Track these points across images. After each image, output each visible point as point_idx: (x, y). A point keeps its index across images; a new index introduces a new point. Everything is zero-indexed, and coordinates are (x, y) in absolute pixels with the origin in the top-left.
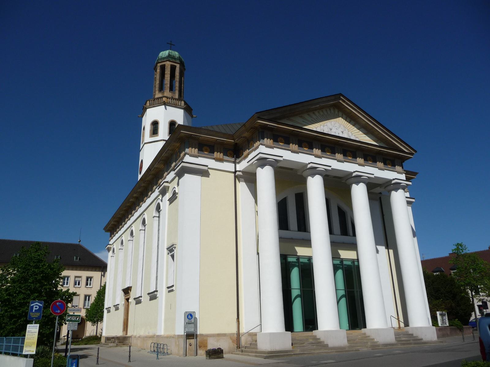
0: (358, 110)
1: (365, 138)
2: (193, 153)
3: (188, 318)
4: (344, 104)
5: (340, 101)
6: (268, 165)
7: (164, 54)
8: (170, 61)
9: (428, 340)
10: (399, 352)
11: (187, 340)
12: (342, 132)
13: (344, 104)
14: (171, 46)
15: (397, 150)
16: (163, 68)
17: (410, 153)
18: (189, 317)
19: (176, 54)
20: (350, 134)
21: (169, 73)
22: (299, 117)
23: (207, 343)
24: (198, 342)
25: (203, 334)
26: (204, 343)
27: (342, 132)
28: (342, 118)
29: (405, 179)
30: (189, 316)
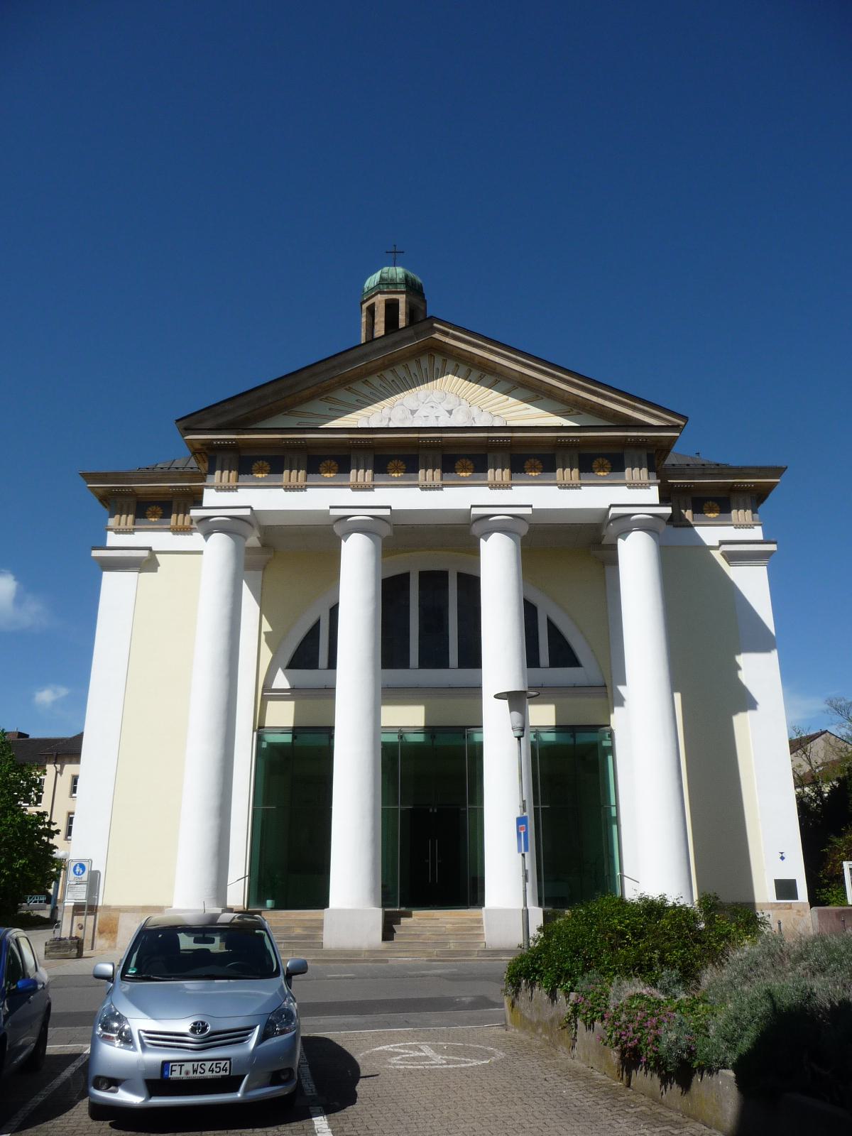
0: (488, 346)
1: (527, 412)
2: (123, 526)
3: (75, 872)
4: (447, 340)
5: (437, 336)
6: (216, 532)
7: (372, 281)
8: (382, 293)
9: (504, 947)
10: (353, 975)
11: (75, 917)
12: (450, 412)
13: (447, 340)
14: (394, 257)
15: (629, 426)
16: (371, 310)
17: (668, 426)
18: (77, 870)
19: (398, 272)
20: (475, 410)
21: (383, 319)
22: (321, 400)
23: (116, 925)
24: (97, 922)
25: (110, 906)
26: (111, 926)
27: (447, 411)
28: (455, 374)
29: (157, 555)
30: (78, 867)
